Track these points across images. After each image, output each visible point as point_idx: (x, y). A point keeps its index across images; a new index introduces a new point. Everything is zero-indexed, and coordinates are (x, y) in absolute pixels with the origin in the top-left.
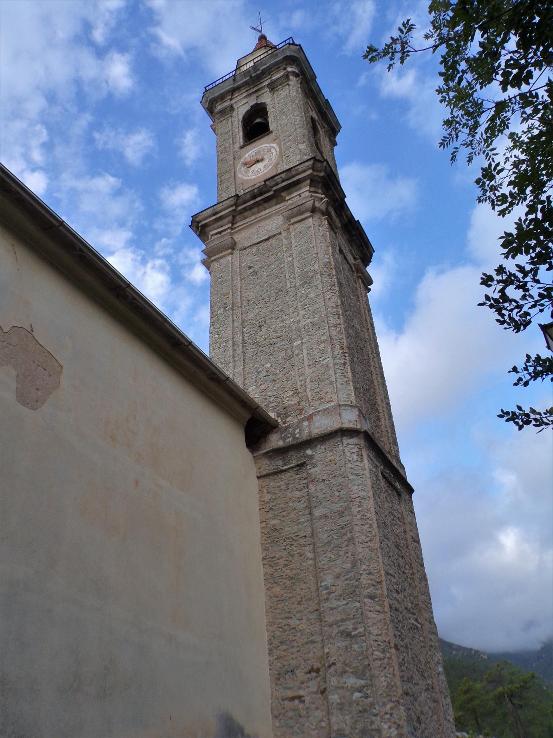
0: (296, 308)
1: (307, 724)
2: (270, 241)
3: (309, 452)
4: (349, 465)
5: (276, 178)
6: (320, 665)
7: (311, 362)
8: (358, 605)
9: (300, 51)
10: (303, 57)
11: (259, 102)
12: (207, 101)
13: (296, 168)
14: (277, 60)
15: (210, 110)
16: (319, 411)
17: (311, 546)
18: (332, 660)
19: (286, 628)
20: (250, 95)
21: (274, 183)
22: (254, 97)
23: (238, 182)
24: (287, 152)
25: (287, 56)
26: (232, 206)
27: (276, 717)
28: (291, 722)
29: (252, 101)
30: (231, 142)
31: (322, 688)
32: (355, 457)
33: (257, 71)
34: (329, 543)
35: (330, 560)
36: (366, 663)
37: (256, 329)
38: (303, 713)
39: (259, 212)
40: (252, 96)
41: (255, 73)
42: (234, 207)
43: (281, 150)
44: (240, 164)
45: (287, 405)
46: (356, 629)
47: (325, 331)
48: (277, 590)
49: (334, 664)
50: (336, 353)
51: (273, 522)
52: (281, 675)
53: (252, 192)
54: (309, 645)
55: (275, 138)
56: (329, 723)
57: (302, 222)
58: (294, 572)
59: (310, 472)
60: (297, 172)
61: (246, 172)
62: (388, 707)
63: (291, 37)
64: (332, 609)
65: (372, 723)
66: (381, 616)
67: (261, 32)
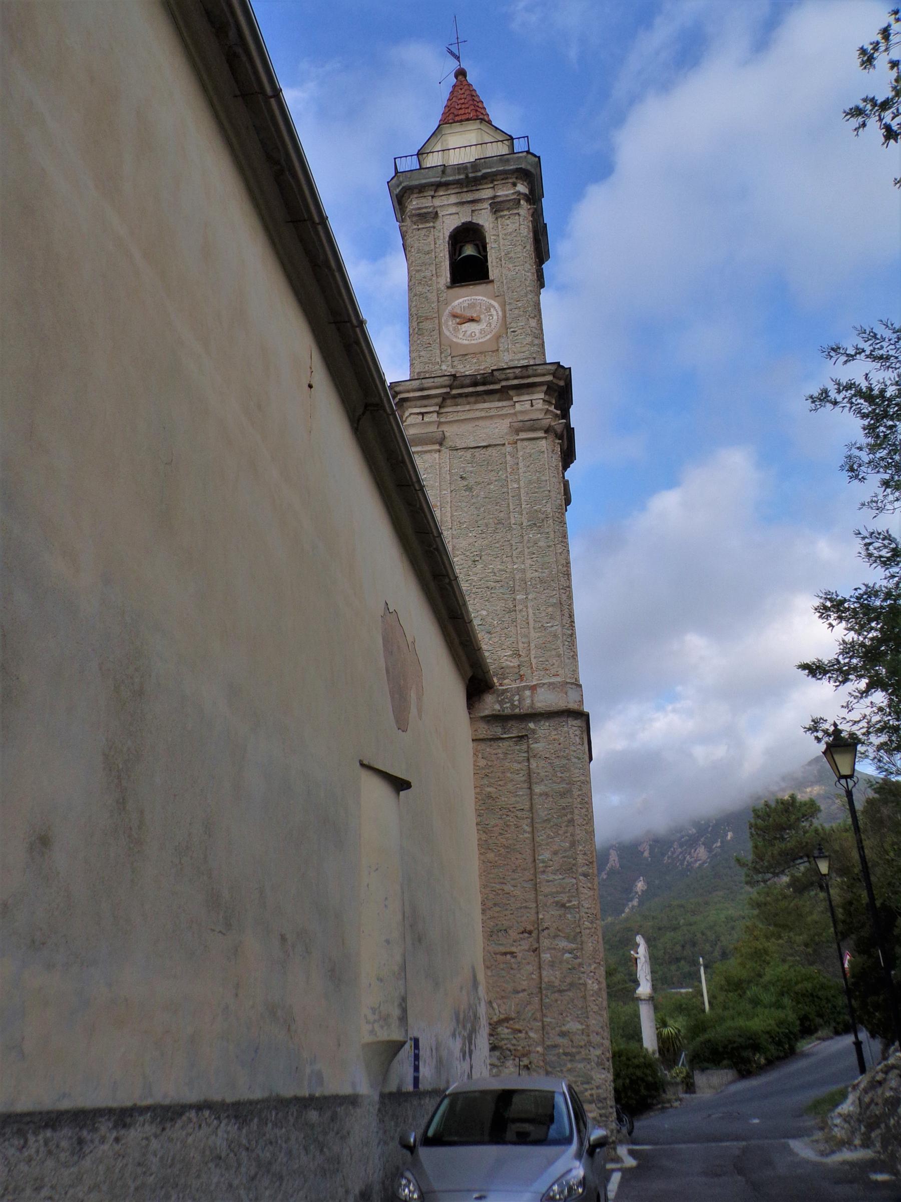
0: (522, 552)
1: (518, 975)
2: (490, 449)
3: (531, 725)
4: (573, 748)
5: (508, 371)
6: (532, 928)
7: (537, 625)
8: (574, 881)
12: (398, 186)
14: (507, 168)
16: (544, 684)
17: (529, 820)
18: (545, 925)
19: (500, 892)
20: (462, 203)
21: (503, 376)
22: (468, 209)
24: (513, 325)
26: (445, 387)
27: (487, 968)
28: (504, 973)
29: (464, 217)
30: (434, 272)
31: (534, 947)
32: (577, 739)
34: (548, 820)
35: (548, 837)
36: (578, 930)
37: (470, 563)
38: (514, 966)
39: (476, 402)
42: (448, 390)
43: (505, 316)
45: (504, 665)
46: (570, 901)
47: (554, 593)
48: (491, 856)
49: (547, 928)
50: (564, 621)
51: (489, 789)
52: (491, 934)
54: (522, 910)
56: (540, 977)
57: (534, 442)
58: (510, 842)
59: (532, 746)
61: (456, 330)
62: (593, 967)
64: (548, 881)
65: (580, 978)
66: (591, 893)
67: (458, 58)
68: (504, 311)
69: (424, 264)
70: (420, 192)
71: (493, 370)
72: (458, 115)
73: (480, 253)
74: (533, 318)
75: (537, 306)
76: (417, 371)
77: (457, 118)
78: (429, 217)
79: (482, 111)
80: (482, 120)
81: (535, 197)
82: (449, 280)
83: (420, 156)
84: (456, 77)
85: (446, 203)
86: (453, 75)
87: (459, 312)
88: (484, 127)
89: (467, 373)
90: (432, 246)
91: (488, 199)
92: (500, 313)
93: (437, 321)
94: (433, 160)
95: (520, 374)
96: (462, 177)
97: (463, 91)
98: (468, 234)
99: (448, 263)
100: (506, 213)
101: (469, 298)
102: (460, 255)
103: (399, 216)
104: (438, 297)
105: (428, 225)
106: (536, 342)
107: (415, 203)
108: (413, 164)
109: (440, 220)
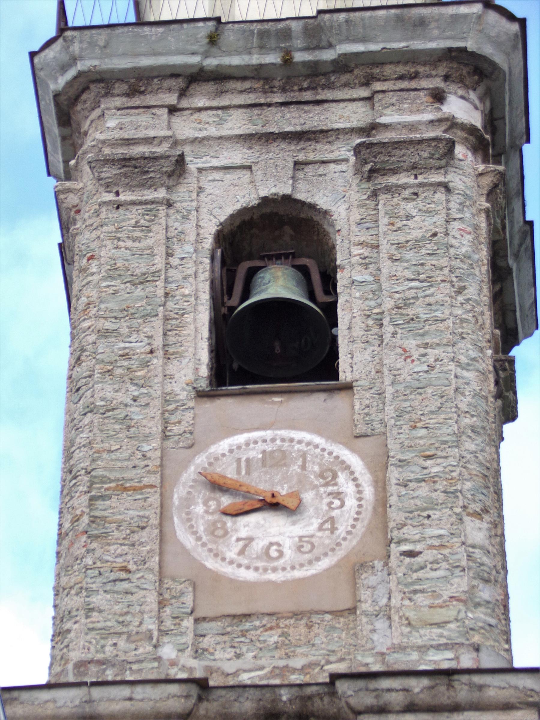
5: (385, 683)
9: (515, 47)
10: (518, 70)
11: (300, 196)
12: (64, 68)
13: (477, 679)
14: (418, 45)
15: (64, 114)
21: (369, 700)
22: (284, 155)
23: (174, 565)
24: (409, 532)
25: (463, 50)
30: (158, 342)
33: (318, 48)
40: (274, 147)
41: (306, 49)
43: (382, 503)
44: (190, 473)
53: (268, 695)
55: (361, 428)
60: (476, 696)
61: (218, 533)
68: (381, 485)
69: (127, 313)
70: (133, 91)
71: (335, 677)
73: (312, 296)
74: (477, 515)
75: (491, 479)
76: (75, 656)
78: (160, 170)
82: (204, 371)
85: (212, 131)
87: (231, 473)
89: (245, 678)
90: (159, 262)
91: (353, 131)
92: (369, 492)
93: (154, 499)
95: (425, 698)
96: (272, 58)
98: (273, 231)
99: (204, 316)
100: (404, 179)
101: (264, 431)
102: (246, 294)
103: (57, 159)
104: (166, 422)
105: (149, 195)
106: (486, 593)
107: (110, 125)
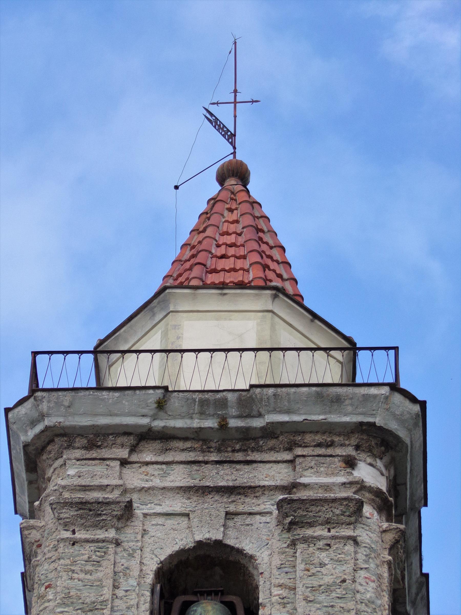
9: (416, 425)
10: (418, 444)
12: (33, 423)
14: (334, 418)
22: (217, 506)
25: (373, 425)
29: (205, 527)
33: (249, 416)
63: (396, 349)
67: (231, 137)
70: (91, 445)
72: (215, 271)
77: (211, 278)
78: (111, 513)
79: (281, 270)
80: (279, 291)
81: (402, 501)
83: (102, 358)
84: (221, 179)
85: (157, 482)
86: (213, 173)
88: (282, 308)
90: (107, 593)
94: (131, 372)
96: (211, 423)
97: (234, 217)
100: (319, 531)
103: (24, 500)
105: (101, 534)
107: (70, 473)
108: (80, 372)
109: (137, 524)
